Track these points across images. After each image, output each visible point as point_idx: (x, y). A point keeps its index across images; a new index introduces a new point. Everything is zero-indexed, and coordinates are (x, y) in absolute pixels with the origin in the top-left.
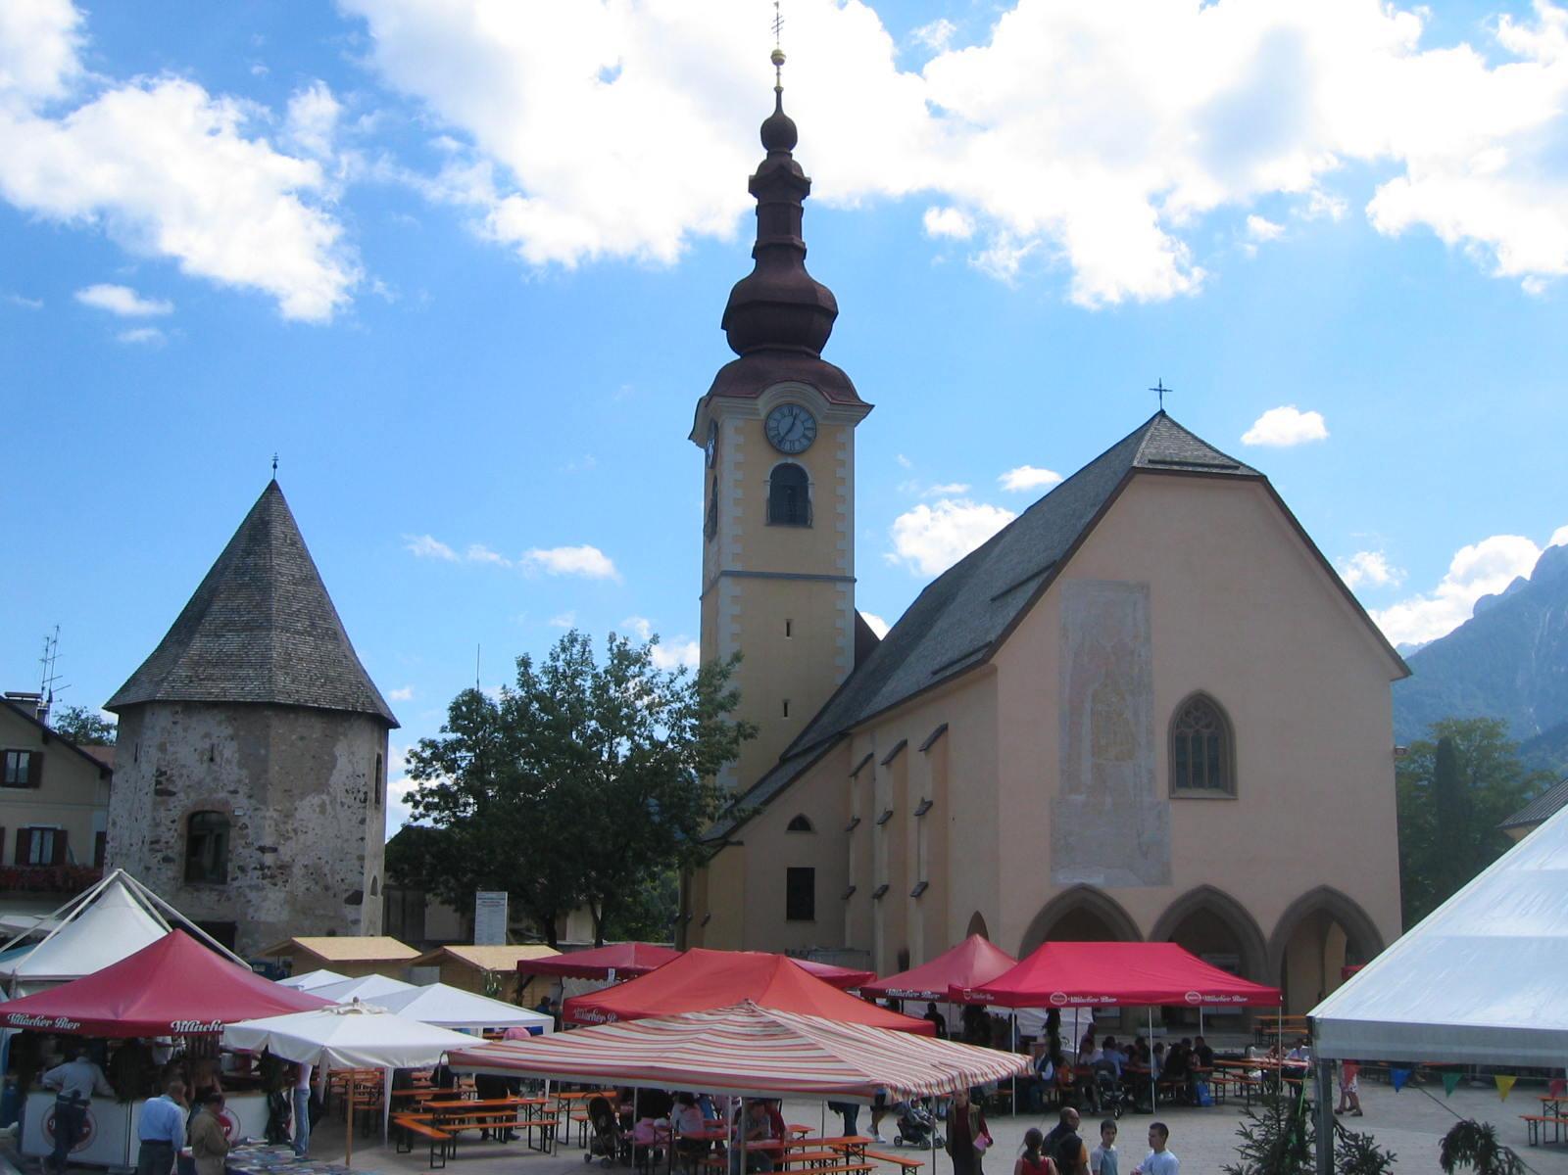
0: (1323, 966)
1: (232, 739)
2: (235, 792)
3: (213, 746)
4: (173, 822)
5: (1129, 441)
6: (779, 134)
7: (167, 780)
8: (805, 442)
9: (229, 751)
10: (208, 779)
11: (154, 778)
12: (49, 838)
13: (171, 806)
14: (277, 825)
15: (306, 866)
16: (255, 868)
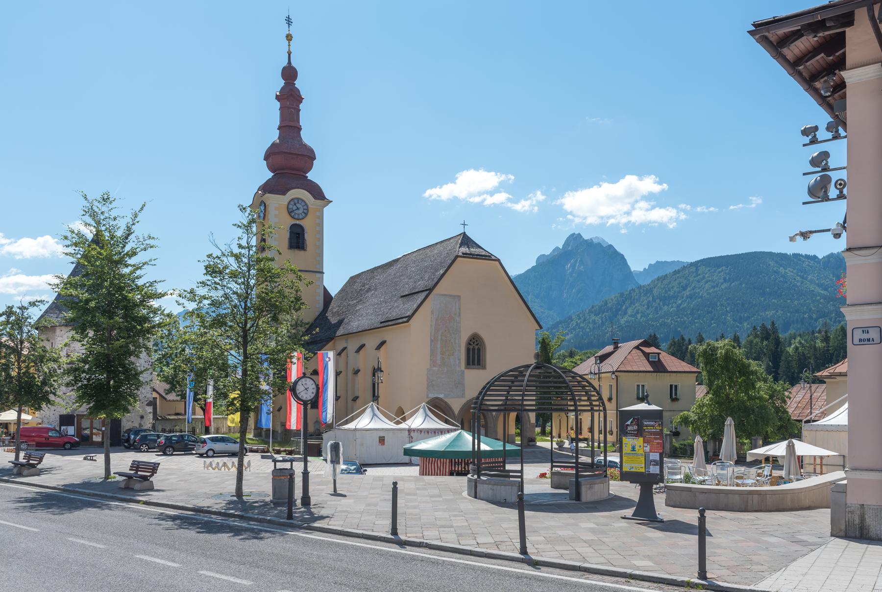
5: (451, 241)
6: (289, 74)
8: (303, 215)
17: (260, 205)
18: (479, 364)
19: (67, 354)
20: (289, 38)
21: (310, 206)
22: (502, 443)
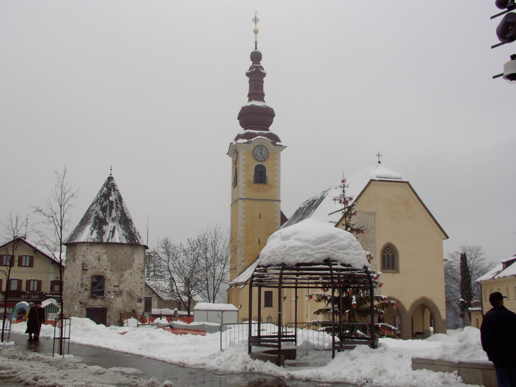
0: (423, 322)
1: (105, 254)
2: (106, 269)
3: (99, 256)
4: (88, 278)
6: (256, 57)
7: (86, 266)
9: (105, 257)
10: (98, 266)
11: (81, 265)
12: (36, 283)
13: (87, 274)
14: (119, 279)
15: (127, 291)
16: (113, 292)
17: (234, 153)
18: (393, 268)
19: (83, 263)
20: (256, 32)
21: (270, 151)
22: (294, 329)
